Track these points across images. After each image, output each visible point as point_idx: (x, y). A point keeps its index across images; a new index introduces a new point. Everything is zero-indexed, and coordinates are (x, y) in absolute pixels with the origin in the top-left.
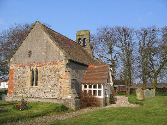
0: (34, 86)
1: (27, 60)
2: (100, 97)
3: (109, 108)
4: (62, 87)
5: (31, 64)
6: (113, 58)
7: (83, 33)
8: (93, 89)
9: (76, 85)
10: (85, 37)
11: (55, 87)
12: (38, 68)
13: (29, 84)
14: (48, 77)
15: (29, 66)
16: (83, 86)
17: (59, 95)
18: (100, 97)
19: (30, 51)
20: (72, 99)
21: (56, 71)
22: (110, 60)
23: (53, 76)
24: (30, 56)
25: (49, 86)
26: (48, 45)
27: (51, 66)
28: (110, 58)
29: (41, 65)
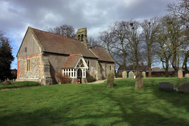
0: (29, 71)
1: (25, 54)
2: (72, 77)
3: (30, 79)
4: (41, 71)
5: (27, 56)
6: (124, 48)
7: (81, 31)
8: (68, 72)
9: (51, 69)
10: (82, 33)
11: (37, 71)
12: (30, 59)
13: (26, 70)
14: (34, 64)
15: (26, 58)
16: (63, 70)
17: (39, 76)
18: (72, 77)
19: (26, 48)
20: (45, 78)
21: (38, 60)
22: (121, 50)
23: (36, 64)
24: (26, 51)
25: (35, 71)
26: (34, 43)
27: (35, 57)
28: (122, 48)
29: (31, 56)
